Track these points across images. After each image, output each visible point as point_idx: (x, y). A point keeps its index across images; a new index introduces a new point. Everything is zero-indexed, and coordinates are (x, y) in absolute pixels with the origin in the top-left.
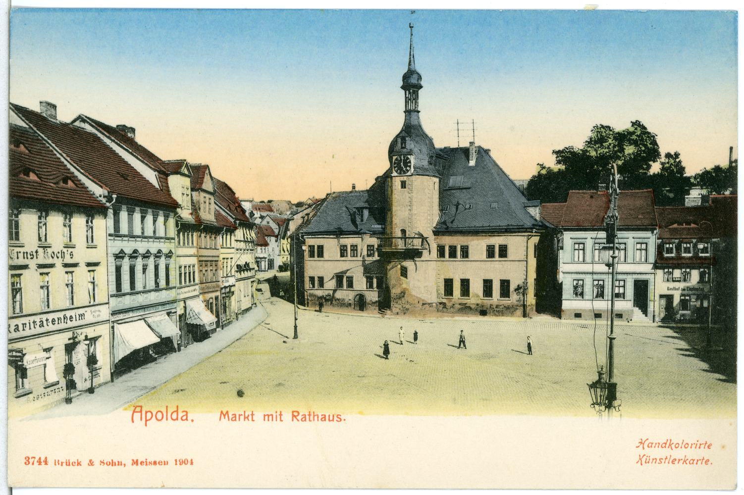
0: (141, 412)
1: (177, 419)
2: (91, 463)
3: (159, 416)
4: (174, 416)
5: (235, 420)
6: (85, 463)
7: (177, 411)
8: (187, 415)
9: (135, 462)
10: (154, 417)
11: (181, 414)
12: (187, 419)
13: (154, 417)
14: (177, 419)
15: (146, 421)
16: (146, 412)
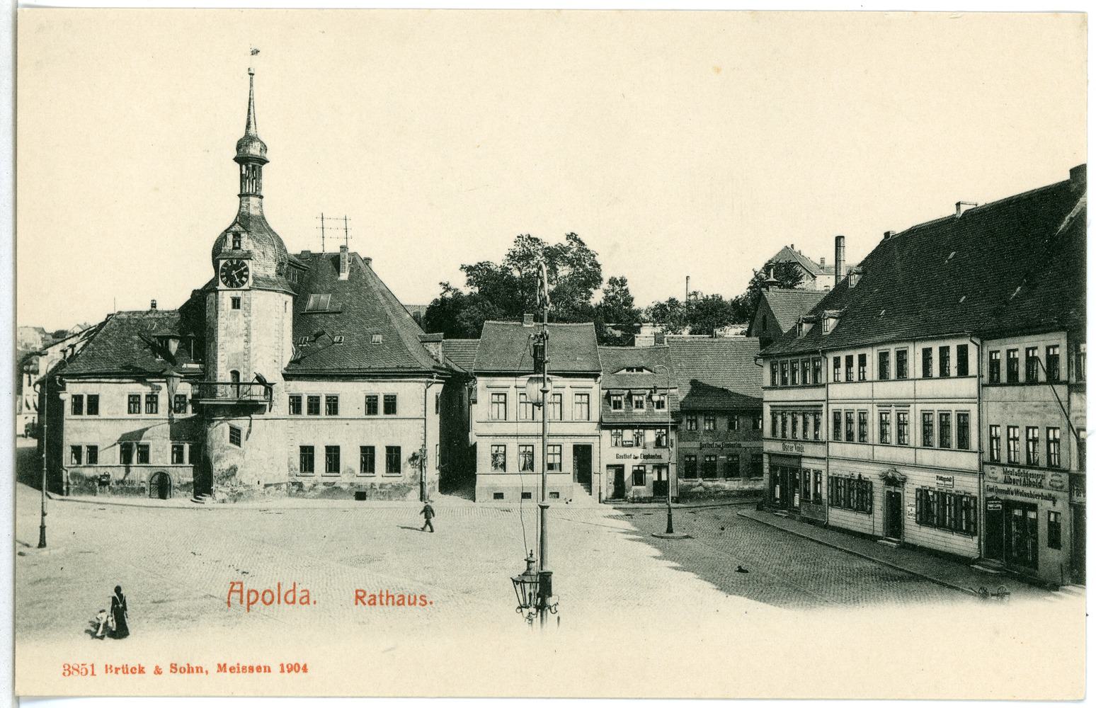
0: (241, 591)
1: (294, 602)
2: (158, 671)
3: (268, 597)
4: (290, 598)
5: (375, 604)
6: (150, 670)
7: (294, 590)
10: (260, 599)
11: (299, 595)
12: (308, 602)
13: (260, 599)
14: (294, 602)
15: (249, 604)
16: (249, 592)
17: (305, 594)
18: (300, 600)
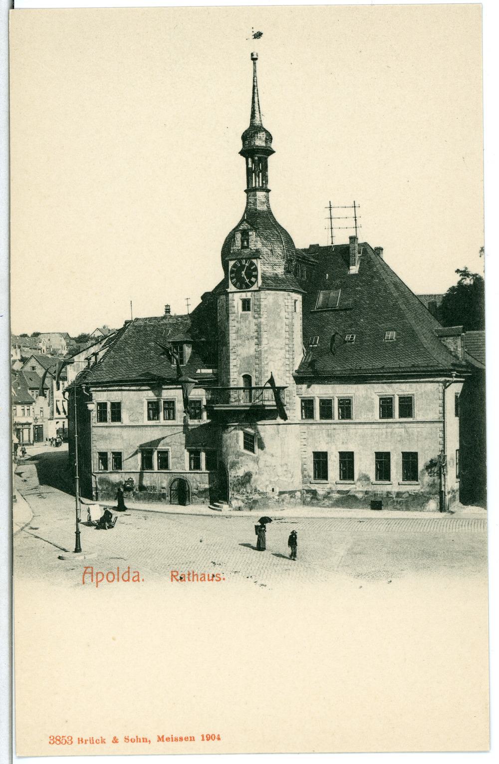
2: (115, 740)
4: (126, 578)
6: (109, 740)
7: (129, 572)
8: (138, 575)
9: (160, 739)
12: (138, 580)
14: (128, 580)
17: (137, 574)
18: (133, 578)
